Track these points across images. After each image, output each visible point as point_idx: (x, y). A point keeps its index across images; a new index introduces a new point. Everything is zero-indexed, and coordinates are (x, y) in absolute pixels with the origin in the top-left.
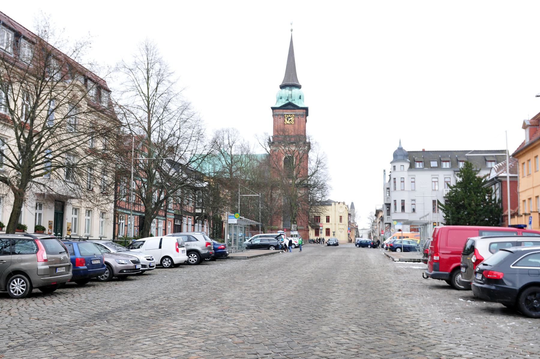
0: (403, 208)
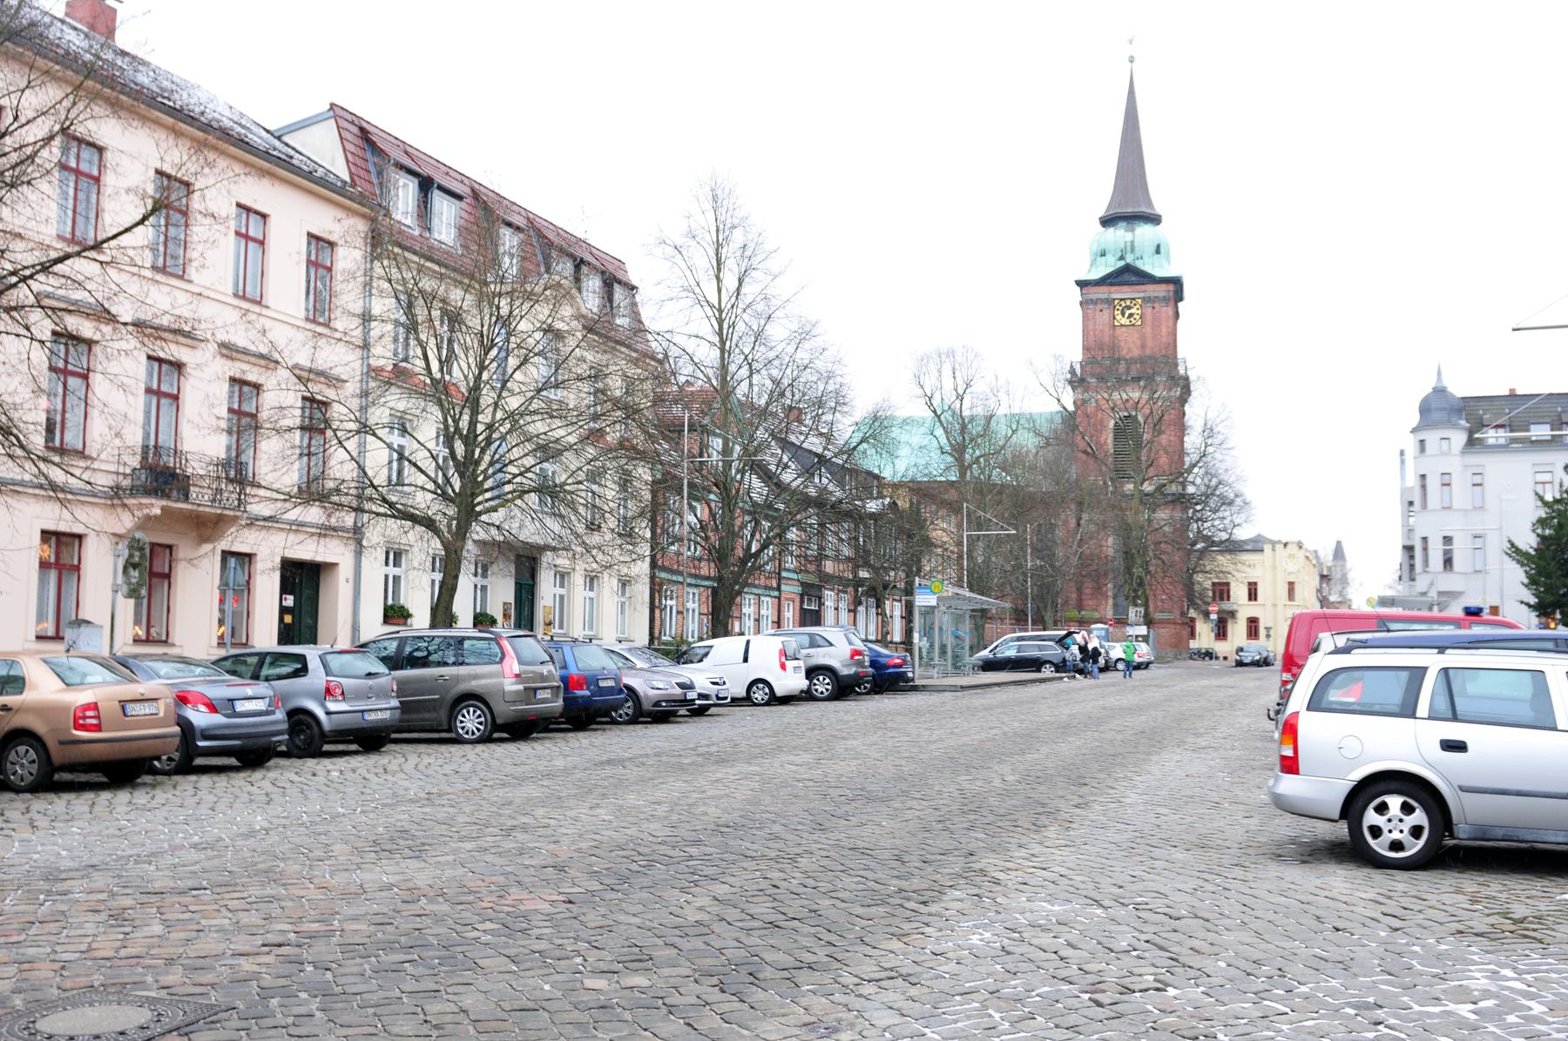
0: (1448, 562)
